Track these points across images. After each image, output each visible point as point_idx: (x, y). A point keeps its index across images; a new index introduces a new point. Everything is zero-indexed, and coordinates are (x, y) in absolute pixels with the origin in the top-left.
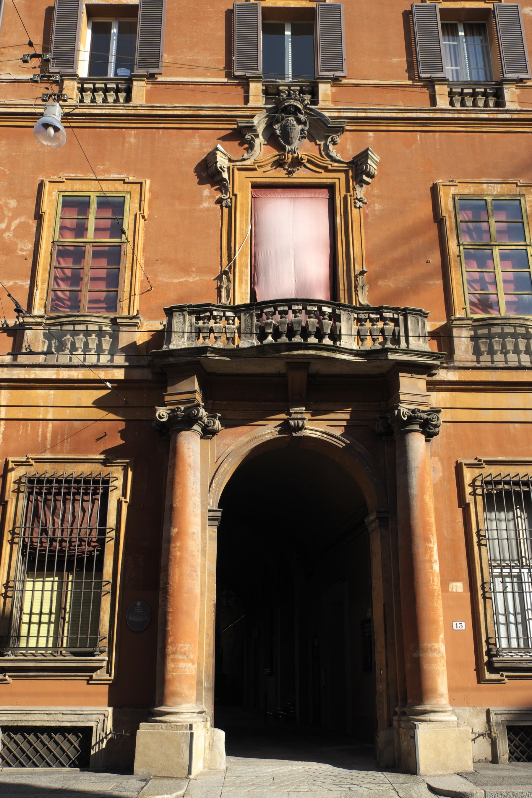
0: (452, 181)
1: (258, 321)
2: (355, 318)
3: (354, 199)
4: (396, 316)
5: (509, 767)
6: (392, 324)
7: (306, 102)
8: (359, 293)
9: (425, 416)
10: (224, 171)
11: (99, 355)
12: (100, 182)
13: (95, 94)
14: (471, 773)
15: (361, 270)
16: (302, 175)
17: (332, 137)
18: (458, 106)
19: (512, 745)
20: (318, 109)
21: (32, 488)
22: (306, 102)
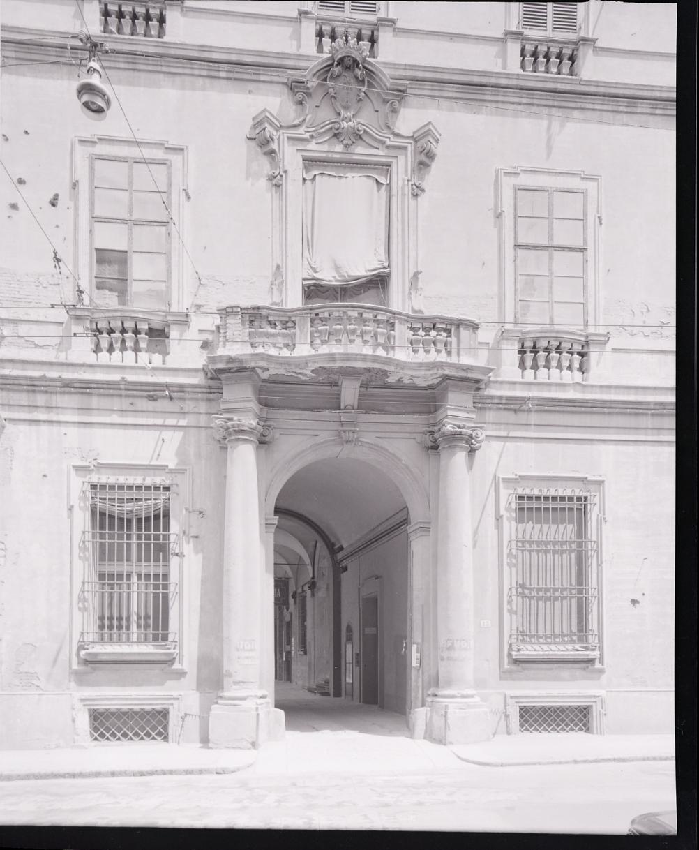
0: (515, 168)
1: (311, 326)
2: (408, 327)
3: (412, 185)
4: (449, 327)
5: (26, 345)
6: (445, 334)
7: (364, 54)
8: (413, 297)
9: (469, 431)
10: (273, 140)
11: (207, 414)
12: (149, 165)
13: (122, 20)
14: (298, 310)
15: (416, 271)
16: (361, 151)
17: (392, 103)
18: (529, 68)
19: (522, 721)
20: (378, 63)
21: (95, 494)
22: (364, 54)
